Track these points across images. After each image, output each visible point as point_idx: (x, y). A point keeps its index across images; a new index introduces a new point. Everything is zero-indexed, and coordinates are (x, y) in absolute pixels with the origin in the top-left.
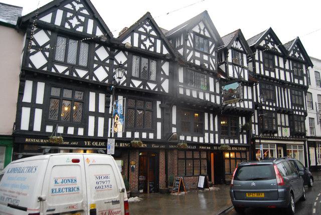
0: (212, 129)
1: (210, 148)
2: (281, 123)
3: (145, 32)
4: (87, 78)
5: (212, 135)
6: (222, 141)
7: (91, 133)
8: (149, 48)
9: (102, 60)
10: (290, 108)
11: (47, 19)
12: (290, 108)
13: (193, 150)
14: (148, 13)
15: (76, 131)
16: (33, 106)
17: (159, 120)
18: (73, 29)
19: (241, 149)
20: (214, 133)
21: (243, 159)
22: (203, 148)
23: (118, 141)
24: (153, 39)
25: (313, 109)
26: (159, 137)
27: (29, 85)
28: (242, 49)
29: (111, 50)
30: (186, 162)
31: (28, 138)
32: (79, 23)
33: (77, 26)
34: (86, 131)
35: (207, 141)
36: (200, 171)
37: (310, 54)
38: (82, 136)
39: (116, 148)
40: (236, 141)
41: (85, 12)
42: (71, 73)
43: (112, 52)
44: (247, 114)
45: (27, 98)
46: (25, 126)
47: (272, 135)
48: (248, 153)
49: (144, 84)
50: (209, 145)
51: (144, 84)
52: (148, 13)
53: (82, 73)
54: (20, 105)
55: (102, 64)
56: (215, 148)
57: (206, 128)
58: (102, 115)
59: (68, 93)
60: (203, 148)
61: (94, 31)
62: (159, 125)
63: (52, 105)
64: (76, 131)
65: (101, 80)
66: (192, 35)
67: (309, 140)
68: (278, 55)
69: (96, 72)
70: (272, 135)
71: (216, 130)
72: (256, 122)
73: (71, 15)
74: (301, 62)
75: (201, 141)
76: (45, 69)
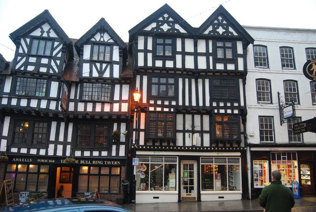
0: (61, 139)
1: (54, 161)
2: (193, 126)
6: (78, 154)
10: (208, 104)
12: (208, 104)
14: (103, 20)
19: (94, 162)
21: (31, 173)
22: (43, 161)
25: (272, 103)
28: (111, 41)
30: (99, 178)
31: (39, 159)
35: (51, 153)
36: (109, 186)
37: (242, 23)
38: (97, 156)
44: (126, 119)
47: (172, 144)
48: (123, 168)
50: (55, 157)
52: (103, 20)
57: (52, 138)
60: (43, 161)
63: (219, 120)
66: (28, 40)
67: (253, 149)
68: (183, 37)
70: (172, 144)
71: (69, 140)
72: (142, 127)
74: (233, 40)
75: (42, 152)
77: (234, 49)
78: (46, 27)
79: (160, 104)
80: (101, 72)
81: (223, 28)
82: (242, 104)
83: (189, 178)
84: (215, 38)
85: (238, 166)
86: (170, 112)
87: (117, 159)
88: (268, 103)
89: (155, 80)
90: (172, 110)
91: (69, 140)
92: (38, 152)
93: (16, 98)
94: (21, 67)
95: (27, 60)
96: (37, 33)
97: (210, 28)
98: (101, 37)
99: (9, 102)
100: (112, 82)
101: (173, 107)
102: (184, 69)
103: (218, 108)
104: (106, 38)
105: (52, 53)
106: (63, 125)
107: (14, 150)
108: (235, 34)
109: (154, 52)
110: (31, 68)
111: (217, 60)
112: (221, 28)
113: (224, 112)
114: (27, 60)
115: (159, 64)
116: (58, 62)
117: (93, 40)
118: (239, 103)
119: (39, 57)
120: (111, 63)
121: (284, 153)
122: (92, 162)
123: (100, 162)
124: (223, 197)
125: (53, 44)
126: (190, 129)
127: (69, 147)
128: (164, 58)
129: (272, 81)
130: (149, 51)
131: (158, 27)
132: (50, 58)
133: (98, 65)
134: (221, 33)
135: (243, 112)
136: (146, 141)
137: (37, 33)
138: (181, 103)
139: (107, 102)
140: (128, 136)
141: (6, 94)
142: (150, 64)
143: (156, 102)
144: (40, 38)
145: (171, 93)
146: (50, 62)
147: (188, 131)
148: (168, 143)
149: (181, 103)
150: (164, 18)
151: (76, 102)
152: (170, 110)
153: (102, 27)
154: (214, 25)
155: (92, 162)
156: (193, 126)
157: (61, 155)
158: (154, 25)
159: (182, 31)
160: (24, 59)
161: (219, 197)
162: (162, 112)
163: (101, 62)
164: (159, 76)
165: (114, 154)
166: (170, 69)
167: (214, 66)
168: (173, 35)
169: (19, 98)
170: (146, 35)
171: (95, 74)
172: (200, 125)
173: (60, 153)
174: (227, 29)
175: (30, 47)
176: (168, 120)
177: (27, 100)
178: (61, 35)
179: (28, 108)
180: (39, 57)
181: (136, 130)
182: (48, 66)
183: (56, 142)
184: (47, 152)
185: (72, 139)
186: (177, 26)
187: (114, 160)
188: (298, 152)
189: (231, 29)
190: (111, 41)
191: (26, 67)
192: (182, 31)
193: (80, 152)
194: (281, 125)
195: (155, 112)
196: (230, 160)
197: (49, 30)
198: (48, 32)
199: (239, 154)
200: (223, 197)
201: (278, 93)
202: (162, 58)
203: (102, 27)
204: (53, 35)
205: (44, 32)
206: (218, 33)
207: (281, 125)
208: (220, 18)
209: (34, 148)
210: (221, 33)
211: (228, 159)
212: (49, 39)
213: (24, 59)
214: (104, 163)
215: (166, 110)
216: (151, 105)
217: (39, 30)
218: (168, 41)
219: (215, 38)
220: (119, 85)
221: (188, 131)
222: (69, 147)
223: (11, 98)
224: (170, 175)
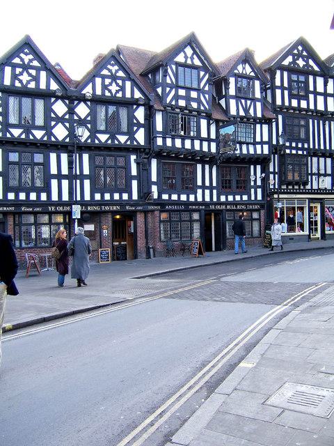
0: (207, 183)
2: (318, 170)
3: (109, 74)
4: (45, 139)
5: (207, 192)
7: (55, 197)
8: (116, 93)
9: (83, 117)
15: (38, 197)
17: (134, 178)
20: (211, 188)
22: (194, 207)
24: (120, 82)
26: (135, 197)
28: (252, 74)
29: (69, 103)
33: (28, 82)
34: (49, 196)
35: (200, 199)
39: (82, 213)
40: (245, 198)
41: (36, 63)
43: (71, 105)
44: (263, 161)
47: (302, 187)
49: (113, 137)
50: (204, 203)
51: (113, 137)
53: (39, 134)
55: (60, 120)
57: (199, 183)
58: (65, 177)
61: (48, 84)
62: (135, 184)
65: (60, 138)
66: (174, 67)
68: (315, 74)
70: (302, 187)
71: (214, 184)
75: (192, 198)
78: (189, 51)
80: (247, 111)
81: (304, 60)
86: (303, 155)
87: (256, 202)
90: (305, 153)
91: (214, 184)
92: (188, 198)
94: (171, 101)
95: (177, 92)
96: (180, 58)
97: (290, 59)
98: (244, 68)
99: (164, 142)
100: (256, 121)
101: (306, 149)
102: (316, 111)
104: (248, 70)
105: (199, 85)
106: (207, 167)
107: (165, 197)
109: (290, 89)
114: (177, 92)
115: (294, 103)
116: (207, 96)
117: (236, 71)
119: (188, 89)
120: (254, 100)
122: (236, 207)
127: (215, 191)
128: (299, 98)
130: (286, 89)
131: (294, 62)
133: (243, 101)
134: (301, 66)
136: (281, 183)
137: (180, 58)
138: (311, 147)
139: (251, 144)
141: (159, 133)
142: (287, 103)
143: (291, 144)
144: (184, 65)
145: (303, 136)
146: (199, 96)
147: (315, 174)
148: (301, 184)
150: (298, 50)
151: (193, 139)
153: (247, 58)
155: (236, 207)
156: (318, 170)
158: (290, 59)
159: (316, 68)
162: (297, 155)
163: (246, 99)
165: (253, 198)
166: (304, 110)
167: (290, 102)
168: (306, 72)
170: (283, 69)
171: (242, 113)
173: (207, 199)
174: (307, 62)
175: (176, 76)
176: (300, 163)
178: (207, 65)
179: (183, 150)
181: (82, 177)
182: (198, 101)
183: (203, 187)
184: (196, 198)
187: (255, 204)
189: (311, 62)
190: (252, 74)
191: (177, 101)
192: (316, 68)
195: (291, 154)
198: (192, 58)
203: (247, 58)
206: (298, 65)
208: (300, 48)
209: (284, 185)
210: (301, 66)
212: (193, 67)
214: (101, 208)
215: (300, 152)
216: (287, 148)
217: (182, 55)
221: (315, 174)
222: (215, 191)
223: (165, 138)
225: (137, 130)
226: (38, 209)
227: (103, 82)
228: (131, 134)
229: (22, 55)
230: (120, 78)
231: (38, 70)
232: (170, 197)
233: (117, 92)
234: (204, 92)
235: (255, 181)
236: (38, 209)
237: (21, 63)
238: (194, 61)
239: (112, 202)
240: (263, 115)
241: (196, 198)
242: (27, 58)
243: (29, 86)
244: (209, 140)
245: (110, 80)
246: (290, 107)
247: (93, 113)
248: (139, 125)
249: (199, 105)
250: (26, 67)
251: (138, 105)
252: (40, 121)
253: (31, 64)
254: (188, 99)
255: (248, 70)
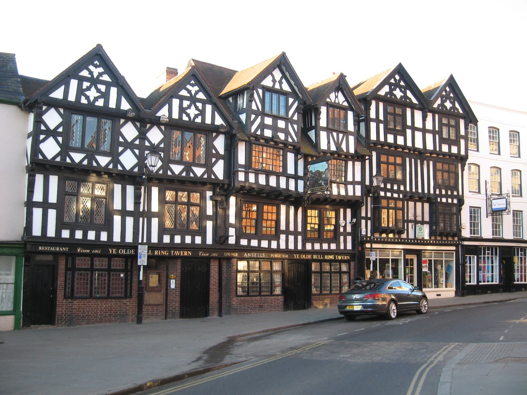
0: (292, 228)
2: (415, 215)
3: (188, 95)
4: (184, 174)
5: (291, 238)
7: (117, 238)
8: (194, 118)
10: (432, 192)
11: (58, 94)
12: (432, 192)
13: (92, 256)
15: (98, 236)
16: (45, 205)
18: (91, 104)
23: (152, 247)
24: (200, 105)
26: (209, 241)
27: (39, 179)
28: (346, 104)
31: (42, 246)
32: (98, 94)
33: (96, 99)
34: (110, 236)
35: (283, 246)
39: (149, 257)
40: (333, 246)
41: (106, 78)
42: (90, 163)
43: (143, 129)
45: (38, 197)
46: (37, 231)
48: (352, 264)
50: (287, 251)
54: (30, 205)
55: (129, 145)
56: (297, 256)
59: (183, 196)
64: (98, 236)
65: (49, 156)
66: (260, 91)
68: (413, 107)
69: (122, 158)
73: (88, 84)
74: (457, 117)
76: (184, 174)
77: (457, 127)
78: (277, 74)
79: (388, 187)
81: (401, 91)
82: (460, 194)
83: (409, 275)
84: (442, 112)
85: (401, 259)
87: (345, 252)
88: (518, 196)
89: (383, 158)
90: (401, 196)
93: (264, 174)
94: (256, 130)
95: (262, 120)
96: (268, 82)
100: (348, 157)
103: (441, 196)
104: (341, 99)
105: (287, 113)
108: (461, 111)
110: (268, 133)
111: (443, 141)
112: (446, 104)
113: (394, 194)
114: (262, 120)
118: (458, 192)
121: (489, 247)
123: (332, 257)
124: (440, 295)
125: (287, 101)
126: (413, 218)
128: (396, 133)
129: (522, 172)
131: (391, 92)
132: (287, 119)
133: (335, 134)
134: (398, 97)
135: (461, 201)
140: (356, 227)
144: (272, 90)
146: (287, 126)
149: (408, 189)
152: (399, 196)
154: (391, 85)
156: (415, 215)
157: (293, 249)
159: (415, 101)
160: (259, 120)
161: (438, 295)
163: (338, 132)
164: (388, 154)
165: (342, 247)
169: (257, 173)
170: (379, 99)
172: (421, 215)
174: (405, 93)
175: (263, 101)
177: (265, 176)
180: (276, 118)
182: (286, 131)
184: (278, 245)
185: (113, 218)
186: (409, 94)
188: (499, 247)
190: (346, 104)
191: (262, 131)
193: (257, 241)
194: (487, 217)
196: (447, 254)
197: (281, 79)
198: (280, 83)
199: (454, 248)
200: (440, 295)
201: (486, 181)
202: (394, 132)
204: (286, 87)
205: (276, 81)
207: (487, 217)
208: (397, 77)
210: (398, 97)
211: (445, 253)
212: (280, 92)
213: (259, 120)
214: (170, 253)
217: (270, 78)
218: (399, 111)
219: (442, 112)
220: (352, 162)
224: (480, 272)
225: (216, 162)
226: (96, 251)
227: (80, 85)
228: (209, 166)
229: (91, 67)
230: (200, 101)
231: (108, 85)
232: (249, 242)
233: (196, 116)
234: (293, 122)
235: (345, 227)
236: (96, 251)
237: (90, 76)
238: (282, 85)
239: (183, 246)
240: (356, 151)
241: (278, 245)
242: (96, 71)
243: (97, 104)
244: (296, 177)
245: (88, 84)
246: (386, 143)
247: (66, 124)
248: (218, 156)
249: (286, 137)
250: (94, 82)
251: (219, 133)
252: (106, 147)
253: (101, 78)
254: (275, 128)
255: (341, 99)
